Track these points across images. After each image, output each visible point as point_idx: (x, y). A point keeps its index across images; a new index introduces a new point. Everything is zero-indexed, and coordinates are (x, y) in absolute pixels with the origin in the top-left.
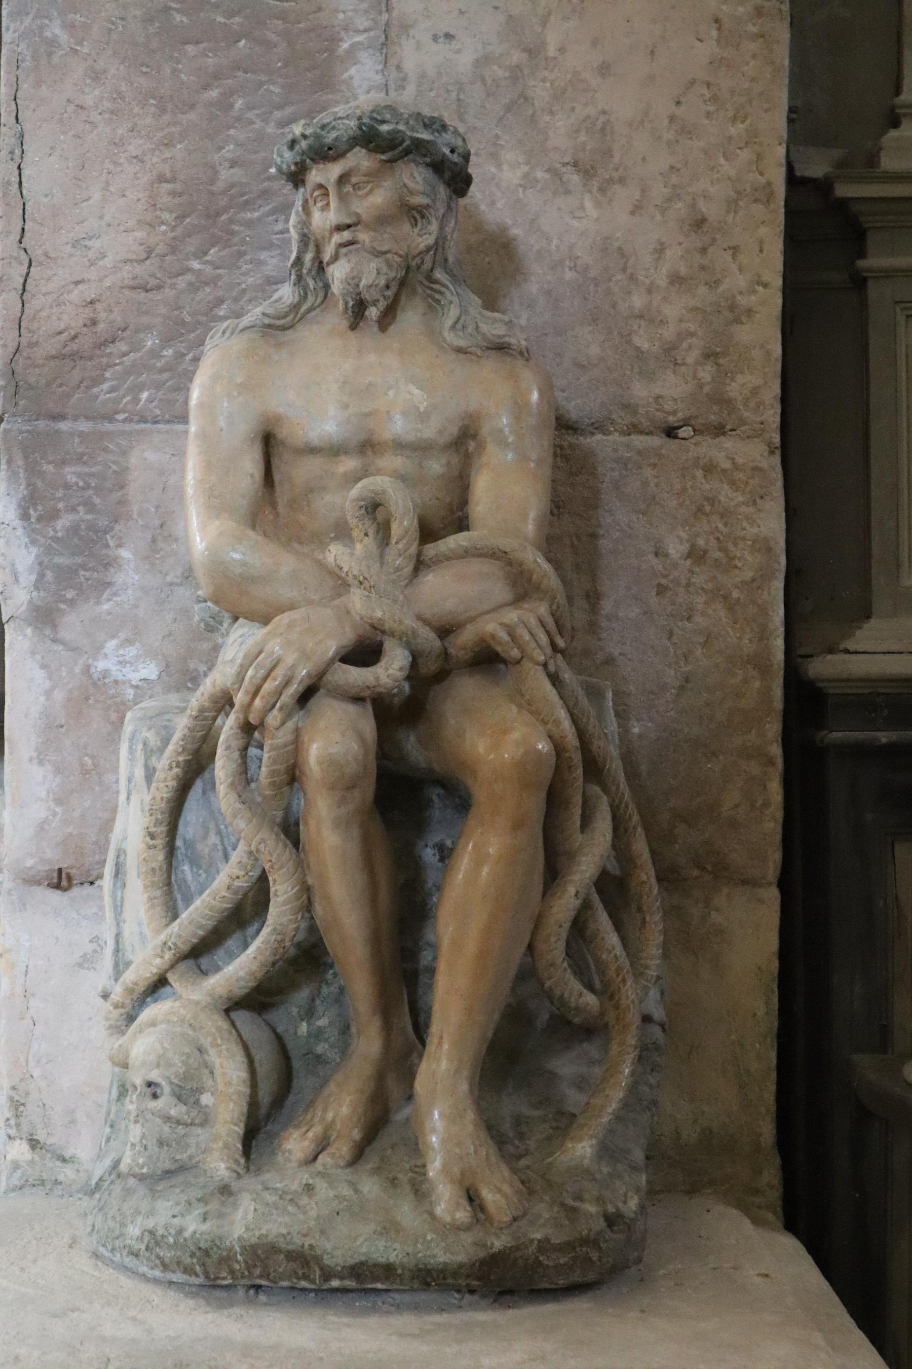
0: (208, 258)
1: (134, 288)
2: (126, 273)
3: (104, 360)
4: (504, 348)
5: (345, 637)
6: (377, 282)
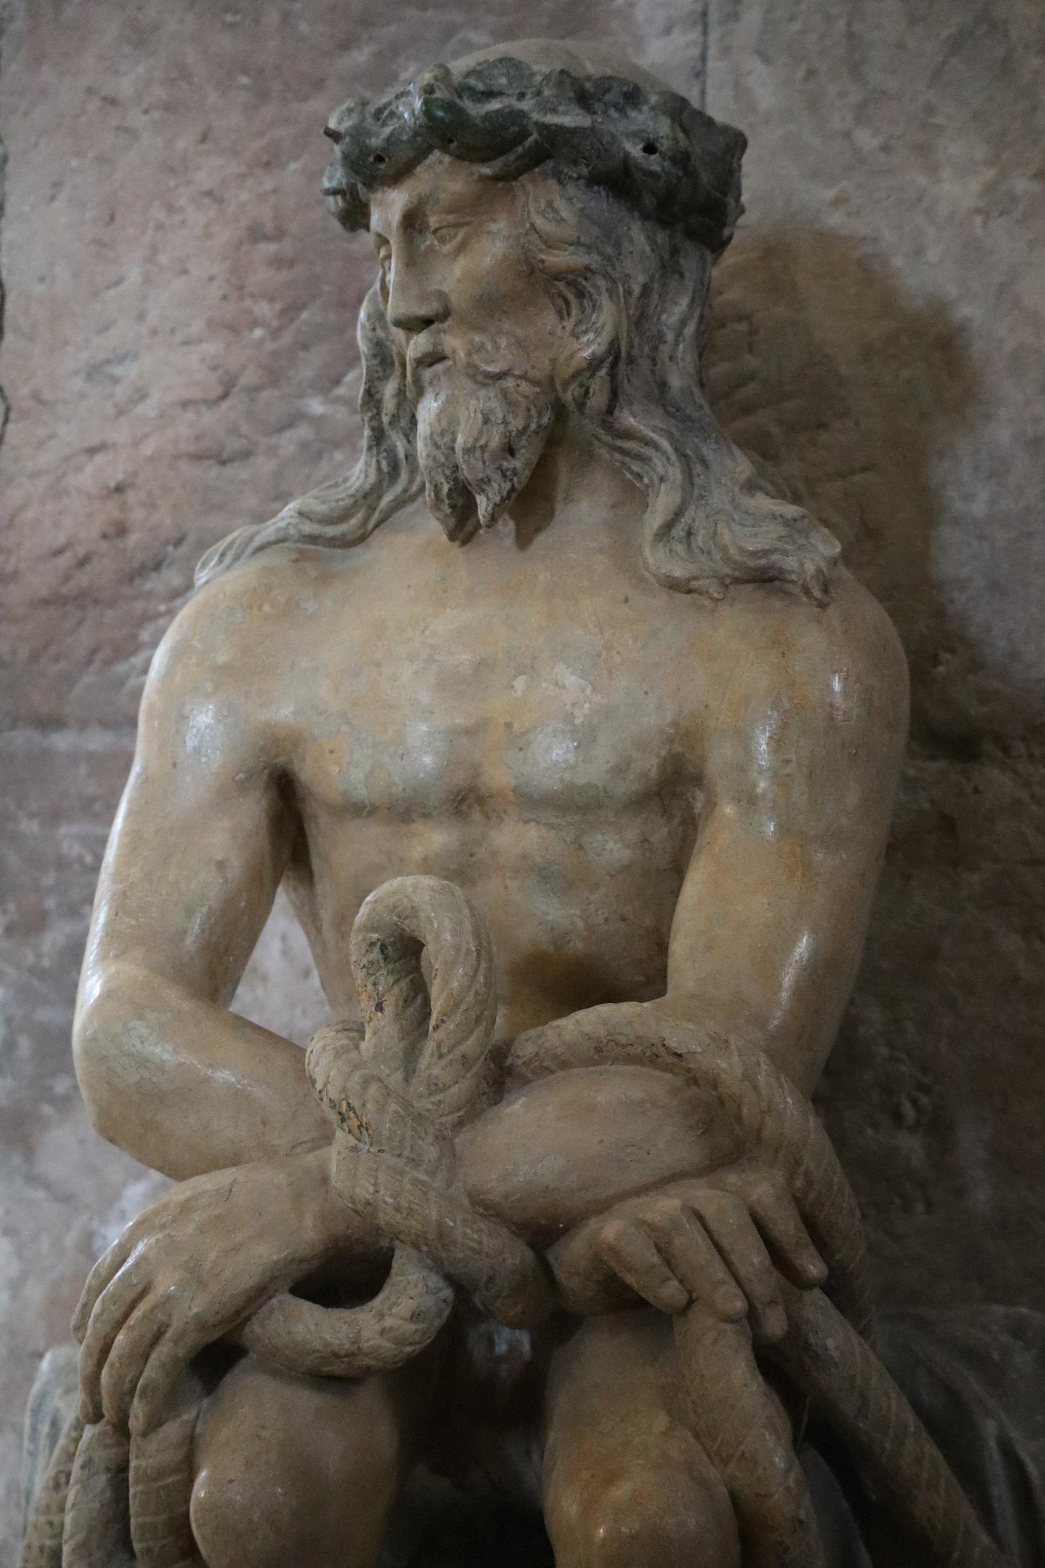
0: (341, 391)
1: (198, 457)
2: (183, 428)
3: (138, 606)
4: (772, 580)
5: (307, 1233)
6: (482, 442)
